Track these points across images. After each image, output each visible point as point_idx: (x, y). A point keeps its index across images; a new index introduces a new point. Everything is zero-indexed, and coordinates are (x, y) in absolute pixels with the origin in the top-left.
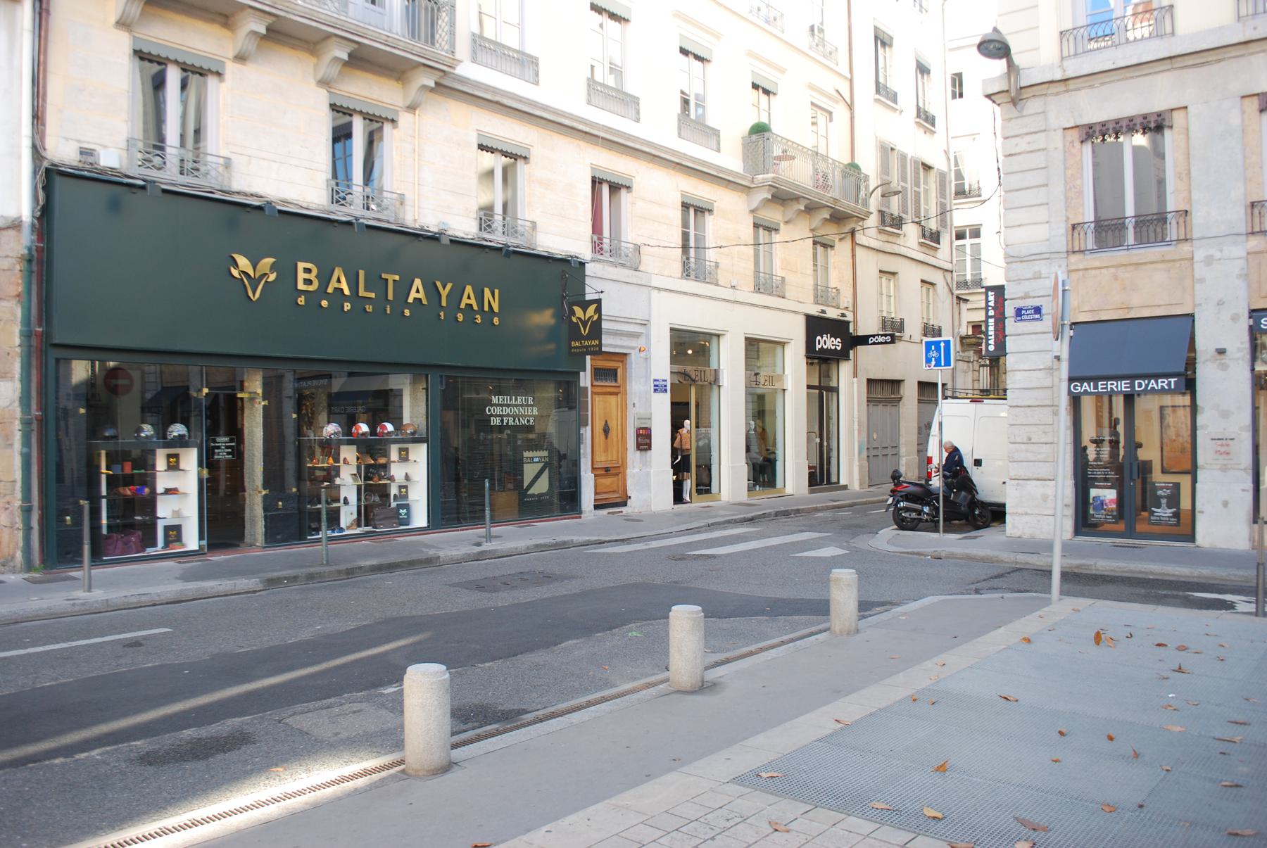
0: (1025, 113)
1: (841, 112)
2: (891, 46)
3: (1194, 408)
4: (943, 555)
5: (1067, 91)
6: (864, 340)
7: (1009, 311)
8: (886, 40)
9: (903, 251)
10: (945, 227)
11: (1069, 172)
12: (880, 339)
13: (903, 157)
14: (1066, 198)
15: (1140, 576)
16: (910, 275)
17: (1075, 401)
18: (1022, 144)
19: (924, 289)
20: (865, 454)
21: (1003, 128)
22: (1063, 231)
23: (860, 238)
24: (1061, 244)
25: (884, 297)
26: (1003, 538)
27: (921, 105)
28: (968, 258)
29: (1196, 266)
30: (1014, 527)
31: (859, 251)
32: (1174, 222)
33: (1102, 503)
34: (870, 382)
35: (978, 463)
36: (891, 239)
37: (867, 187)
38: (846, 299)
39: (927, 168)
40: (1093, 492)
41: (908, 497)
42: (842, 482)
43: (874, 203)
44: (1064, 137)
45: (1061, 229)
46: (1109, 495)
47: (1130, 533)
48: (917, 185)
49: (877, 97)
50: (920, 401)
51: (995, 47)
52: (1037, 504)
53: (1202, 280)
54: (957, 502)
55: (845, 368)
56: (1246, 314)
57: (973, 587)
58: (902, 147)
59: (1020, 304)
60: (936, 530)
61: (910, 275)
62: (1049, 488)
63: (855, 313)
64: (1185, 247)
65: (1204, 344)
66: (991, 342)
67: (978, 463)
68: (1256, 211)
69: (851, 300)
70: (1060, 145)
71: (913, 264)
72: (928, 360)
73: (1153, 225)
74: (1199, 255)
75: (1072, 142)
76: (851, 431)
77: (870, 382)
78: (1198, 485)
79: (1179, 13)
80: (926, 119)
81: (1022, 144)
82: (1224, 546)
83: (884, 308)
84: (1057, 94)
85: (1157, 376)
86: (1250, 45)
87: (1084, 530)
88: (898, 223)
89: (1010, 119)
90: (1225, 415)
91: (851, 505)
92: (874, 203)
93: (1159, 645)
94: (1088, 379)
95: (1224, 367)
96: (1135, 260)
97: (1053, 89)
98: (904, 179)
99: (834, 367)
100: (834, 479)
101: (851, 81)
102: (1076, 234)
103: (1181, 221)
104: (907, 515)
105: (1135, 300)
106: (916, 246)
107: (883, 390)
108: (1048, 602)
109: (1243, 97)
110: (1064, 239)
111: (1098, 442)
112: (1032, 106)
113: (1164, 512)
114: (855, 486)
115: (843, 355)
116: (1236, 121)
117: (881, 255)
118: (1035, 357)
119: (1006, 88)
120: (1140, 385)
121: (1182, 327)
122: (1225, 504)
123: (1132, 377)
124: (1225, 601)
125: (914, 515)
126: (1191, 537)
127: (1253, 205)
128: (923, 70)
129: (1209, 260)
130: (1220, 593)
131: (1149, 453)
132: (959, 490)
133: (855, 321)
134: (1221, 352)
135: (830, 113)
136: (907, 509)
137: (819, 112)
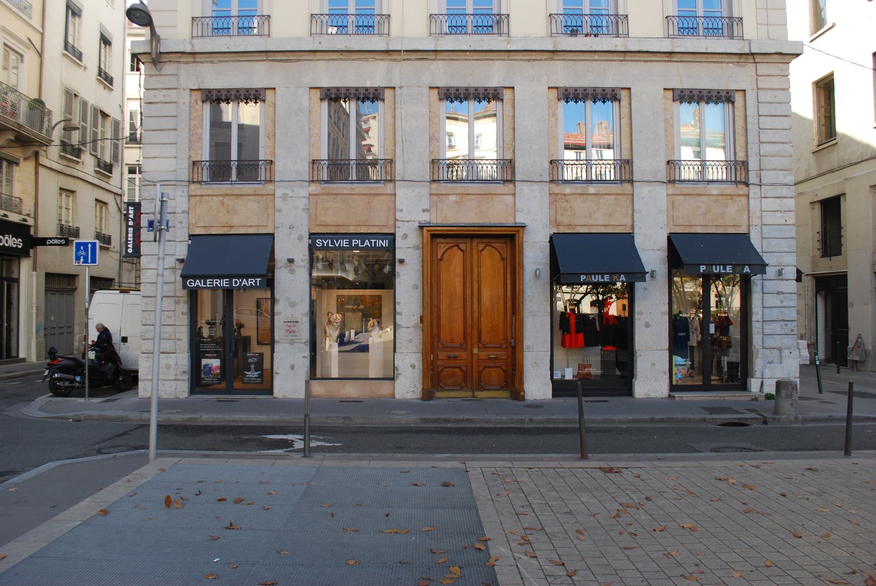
0: (163, 73)
1: (31, 57)
2: (79, 16)
3: (273, 300)
4: (83, 417)
5: (195, 62)
6: (43, 241)
7: (144, 223)
8: (76, 11)
9: (81, 175)
10: (117, 161)
11: (193, 122)
12: (56, 242)
13: (85, 104)
14: (190, 141)
15: (233, 424)
16: (86, 195)
17: (193, 296)
18: (159, 96)
19: (98, 206)
20: (42, 333)
21: (145, 80)
22: (186, 165)
23: (43, 160)
24: (184, 175)
25: (64, 209)
26: (136, 399)
27: (102, 67)
28: (137, 188)
29: (276, 200)
30: (145, 390)
31: (41, 170)
32: (263, 168)
33: (210, 369)
34: (48, 276)
35: (124, 340)
36: (71, 164)
37: (50, 121)
38: (28, 207)
39: (105, 115)
40: (204, 361)
41: (62, 369)
42: (22, 355)
43: (57, 135)
44: (191, 96)
45: (185, 164)
46: (215, 363)
47: (230, 390)
48: (95, 126)
49: (65, 52)
50: (47, 290)
51: (138, 15)
52: (162, 371)
53: (280, 211)
54: (108, 371)
55: (25, 265)
56: (307, 237)
57: (97, 447)
58: (84, 95)
59: (151, 217)
60: (83, 396)
61: (86, 195)
62: (171, 360)
63: (36, 218)
64: (270, 186)
65: (281, 255)
66: (130, 246)
67: (124, 340)
68: (315, 166)
69: (32, 209)
70: (187, 101)
71: (90, 187)
72: (78, 258)
73: (250, 169)
74: (279, 193)
75: (196, 101)
76: (30, 314)
77: (48, 276)
78: (275, 354)
79: (273, 20)
80: (106, 79)
81: (159, 96)
82: (292, 396)
83: (64, 218)
84: (187, 63)
85: (247, 277)
86: (317, 54)
87: (198, 389)
88: (78, 152)
89: (151, 76)
90: (293, 305)
91: (24, 376)
92: (57, 135)
93: (220, 500)
94: (200, 277)
95: (292, 272)
96: (236, 192)
97: (184, 59)
98: (84, 119)
99: (15, 264)
100: (14, 354)
101: (42, 34)
102: (196, 169)
103: (268, 167)
104: (61, 384)
105: (236, 221)
106: (92, 173)
107: (60, 284)
108: (145, 460)
109: (311, 88)
110: (187, 171)
111: (211, 324)
112: (169, 68)
113: (252, 374)
114: (34, 359)
115: (23, 253)
116: (306, 103)
117: (61, 177)
118: (161, 260)
119: (149, 51)
120: (236, 282)
121: (265, 242)
122: (292, 367)
123: (230, 277)
124: (287, 440)
125: (67, 384)
126: (270, 391)
127: (314, 162)
128: (105, 41)
129: (285, 197)
130: (285, 434)
131: (250, 331)
132: (107, 362)
133: (36, 226)
134: (291, 261)
135: (22, 56)
136: (60, 379)
137: (11, 52)
